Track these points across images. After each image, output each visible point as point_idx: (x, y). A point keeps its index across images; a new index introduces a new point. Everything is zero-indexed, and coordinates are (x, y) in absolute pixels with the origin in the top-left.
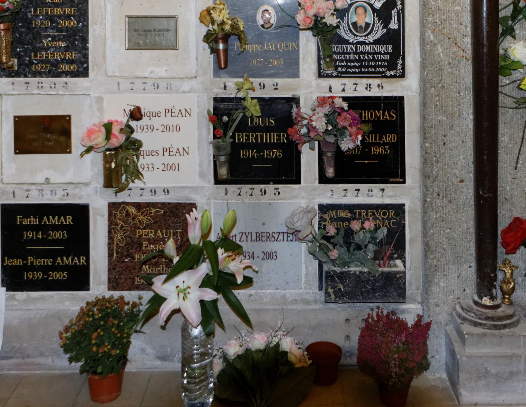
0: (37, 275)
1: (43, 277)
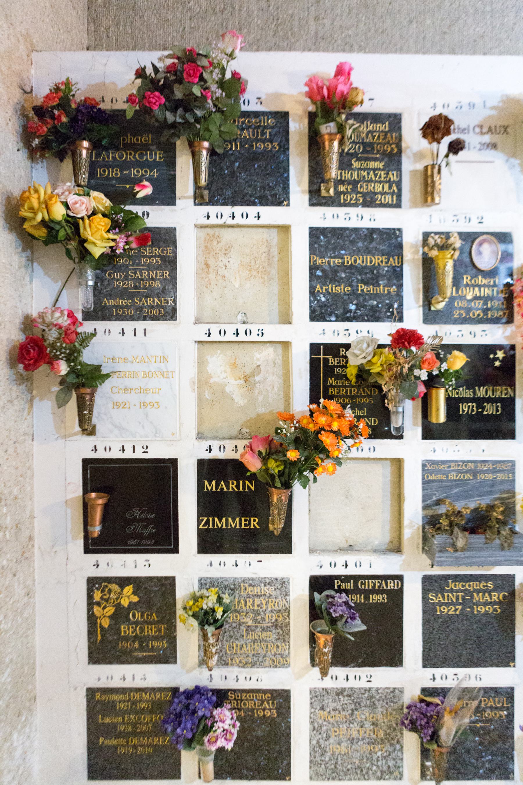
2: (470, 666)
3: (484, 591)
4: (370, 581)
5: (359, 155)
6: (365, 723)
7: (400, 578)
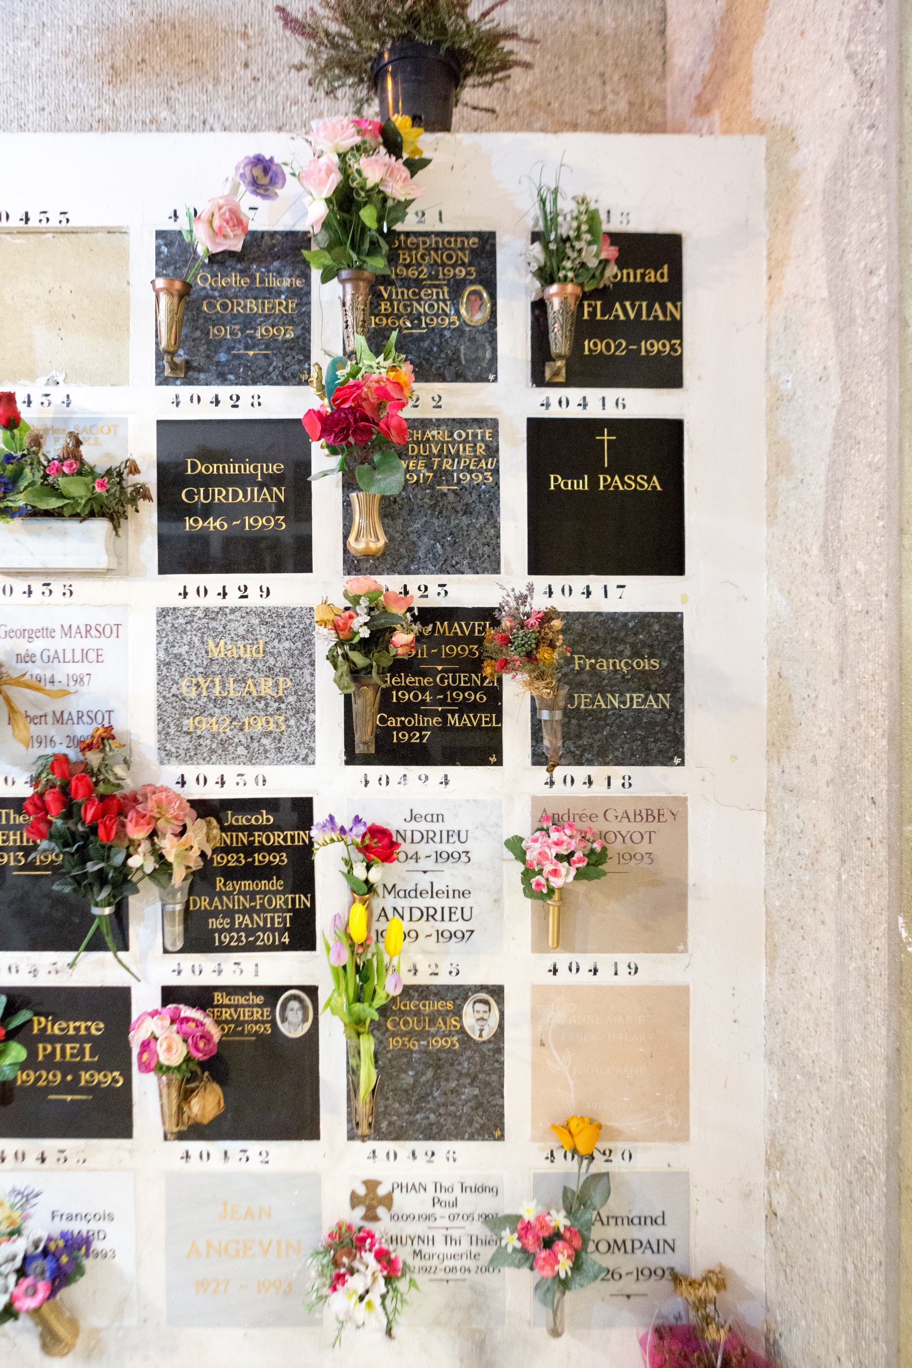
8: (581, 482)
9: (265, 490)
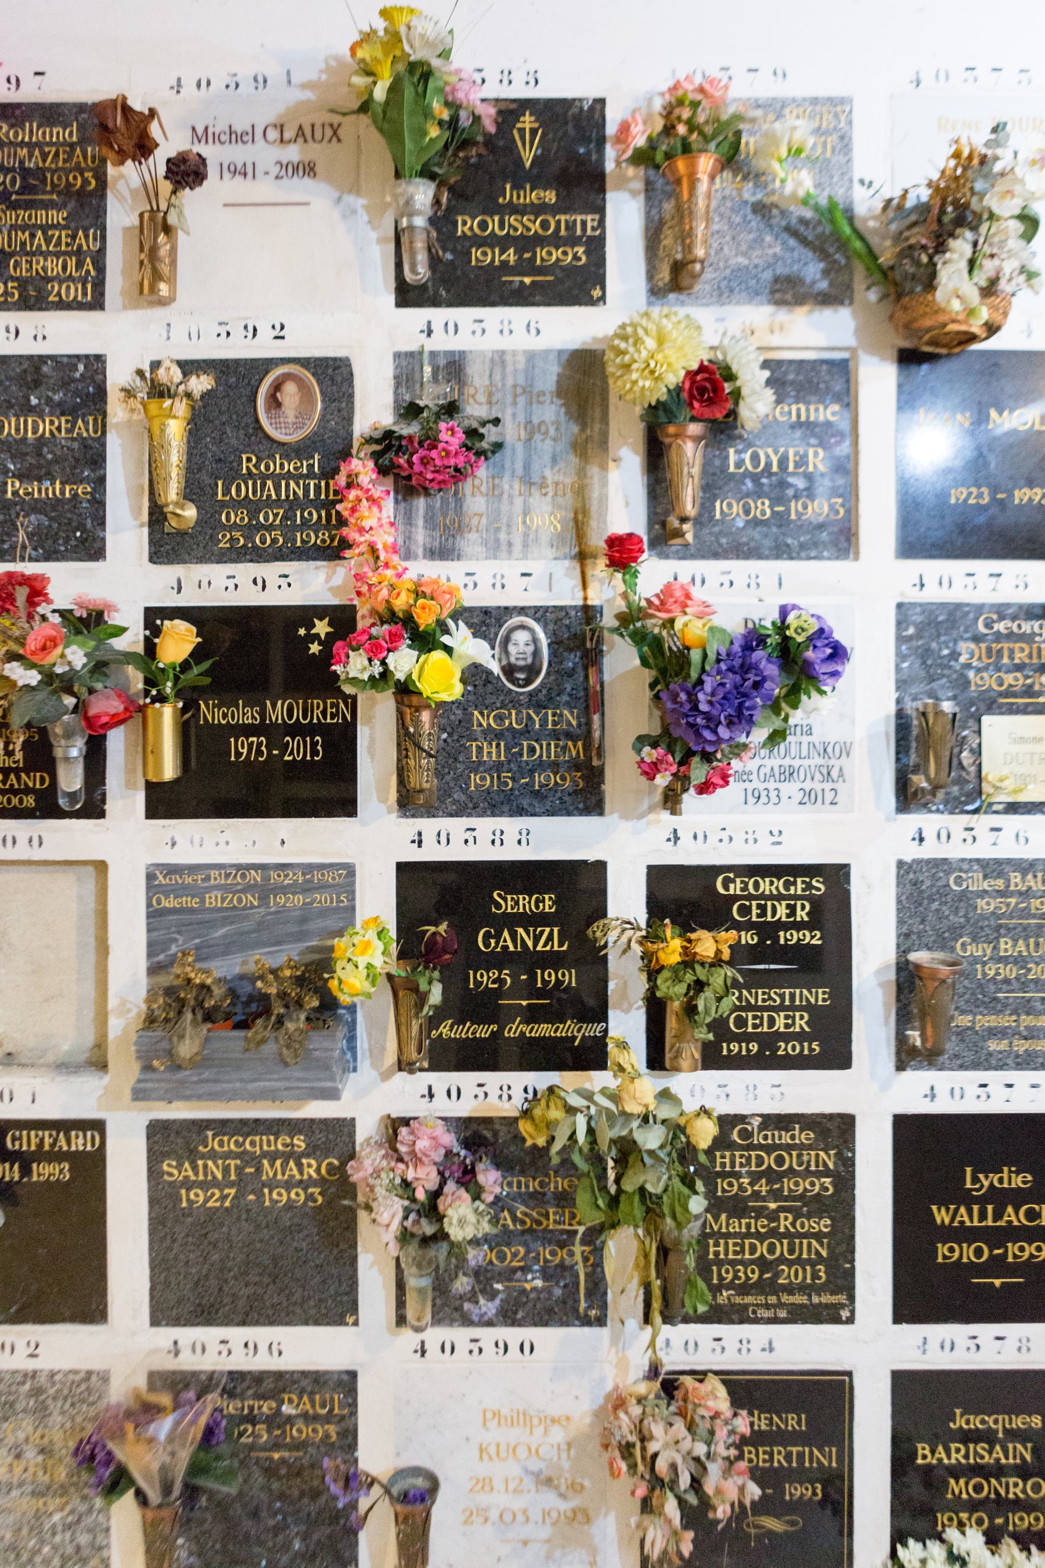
0: (745, 1273)
1: (761, 1276)
2: (257, 1323)
3: (287, 1157)
4: (33, 1133)
5: (14, 197)
6: (25, 1448)
7: (98, 1126)
8: (522, 193)
9: (292, 1164)
